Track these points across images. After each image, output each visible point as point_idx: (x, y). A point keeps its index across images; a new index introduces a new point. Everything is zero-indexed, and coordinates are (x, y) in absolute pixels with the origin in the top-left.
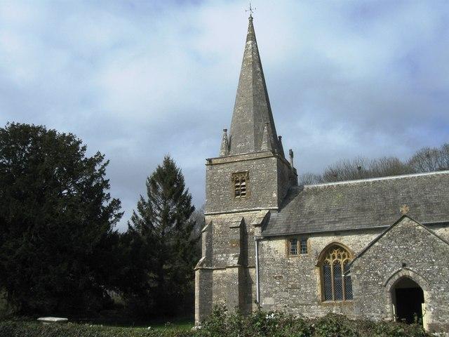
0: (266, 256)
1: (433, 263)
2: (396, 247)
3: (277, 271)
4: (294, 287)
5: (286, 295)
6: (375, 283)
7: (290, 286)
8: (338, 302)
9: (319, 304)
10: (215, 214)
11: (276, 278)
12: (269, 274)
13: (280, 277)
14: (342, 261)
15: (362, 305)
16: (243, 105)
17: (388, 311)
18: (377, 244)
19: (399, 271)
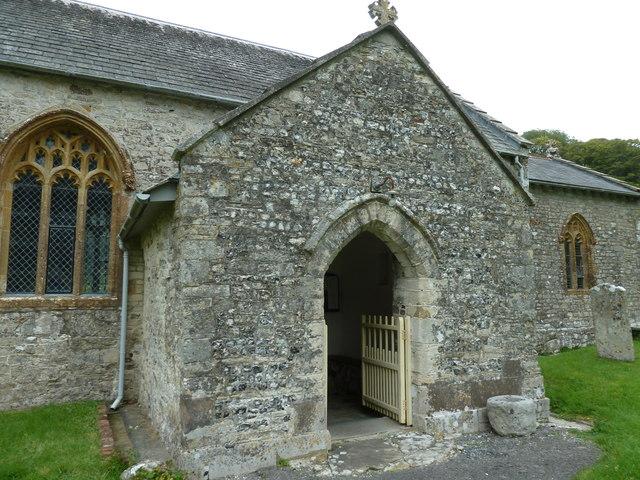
1: (449, 193)
2: (358, 122)
6: (276, 239)
8: (59, 298)
14: (84, 176)
15: (219, 323)
17: (315, 344)
18: (295, 96)
19: (362, 205)
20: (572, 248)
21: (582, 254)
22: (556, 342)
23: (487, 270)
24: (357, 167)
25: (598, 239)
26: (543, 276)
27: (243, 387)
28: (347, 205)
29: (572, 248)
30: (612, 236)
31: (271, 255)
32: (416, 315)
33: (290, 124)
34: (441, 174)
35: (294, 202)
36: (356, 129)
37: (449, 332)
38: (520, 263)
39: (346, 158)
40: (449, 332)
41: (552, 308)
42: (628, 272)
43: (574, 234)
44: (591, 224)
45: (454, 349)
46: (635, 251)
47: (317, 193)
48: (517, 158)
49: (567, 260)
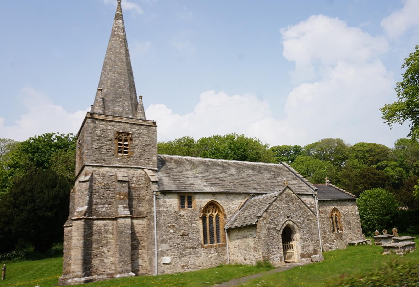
0: (162, 208)
1: (300, 216)
2: (284, 206)
3: (171, 220)
4: (184, 234)
5: (178, 241)
7: (181, 234)
9: (202, 247)
10: (97, 166)
11: (170, 227)
12: (165, 223)
13: (174, 226)
14: (215, 214)
16: (118, 74)
18: (274, 203)
20: (334, 219)
21: (338, 221)
22: (331, 250)
23: (309, 231)
24: (284, 214)
25: (342, 215)
26: (325, 229)
27: (272, 254)
28: (284, 222)
29: (334, 219)
30: (347, 213)
31: (274, 232)
32: (296, 241)
33: (274, 208)
34: (298, 213)
35: (276, 222)
36: (284, 207)
37: (303, 244)
38: (315, 229)
39: (282, 213)
40: (303, 244)
41: (329, 239)
42: (354, 225)
43: (334, 214)
44: (339, 210)
45: (304, 247)
46: (355, 218)
47: (279, 220)
48: (314, 195)
49: (333, 223)
